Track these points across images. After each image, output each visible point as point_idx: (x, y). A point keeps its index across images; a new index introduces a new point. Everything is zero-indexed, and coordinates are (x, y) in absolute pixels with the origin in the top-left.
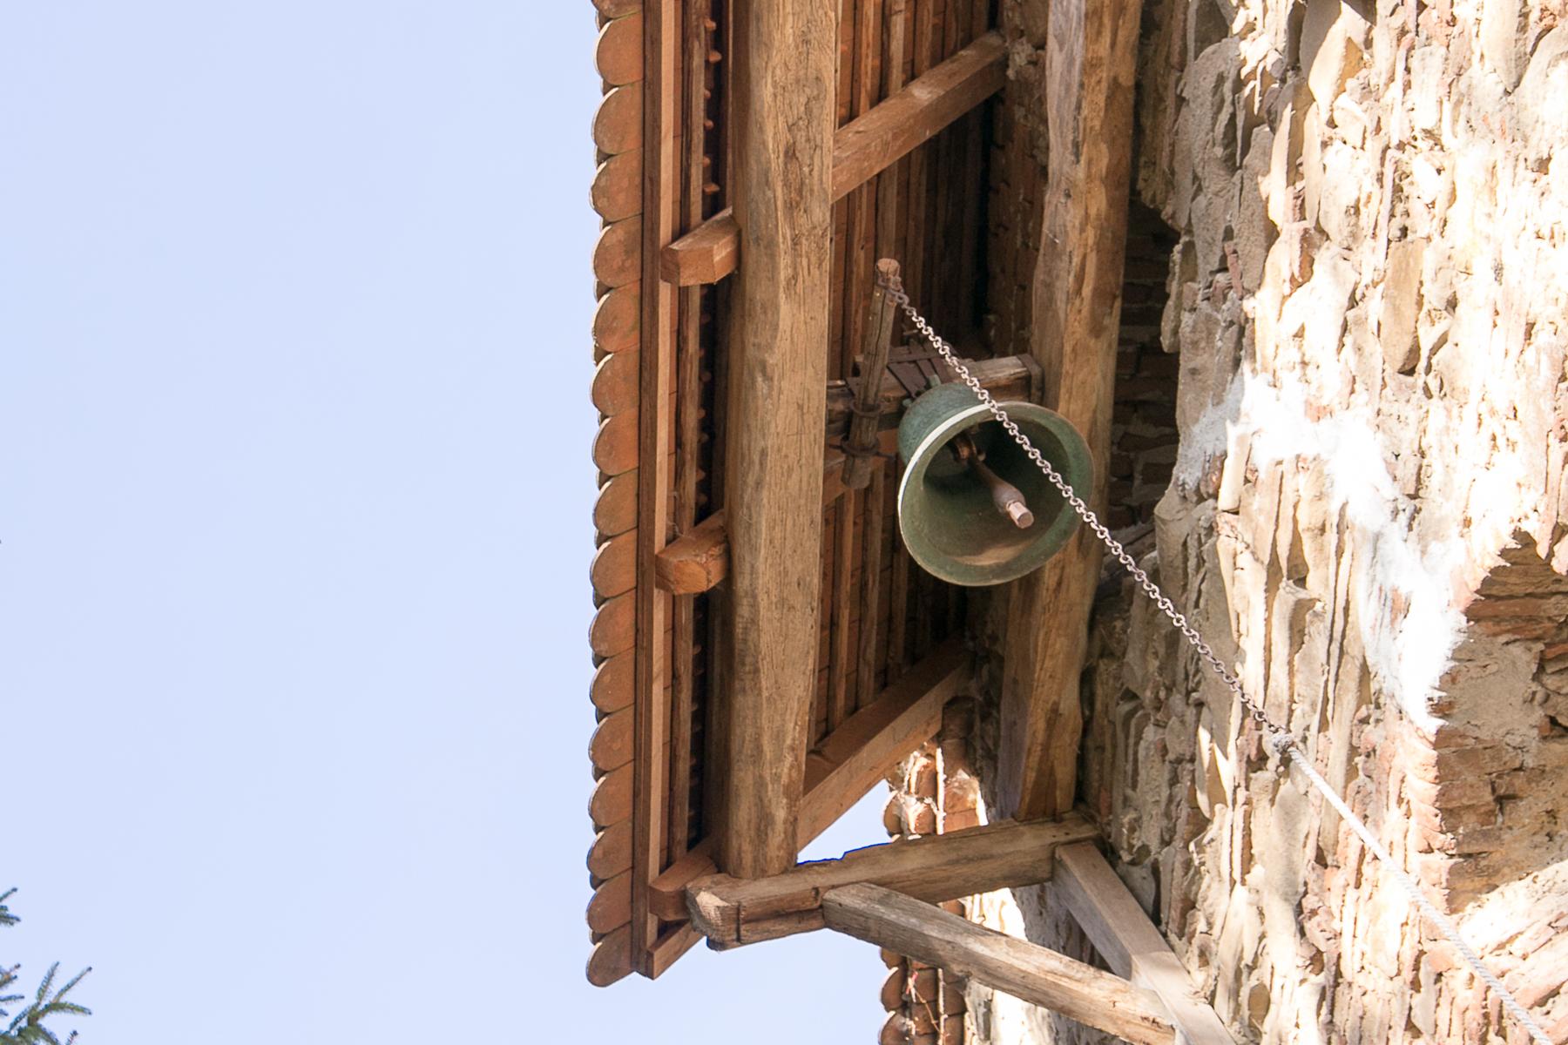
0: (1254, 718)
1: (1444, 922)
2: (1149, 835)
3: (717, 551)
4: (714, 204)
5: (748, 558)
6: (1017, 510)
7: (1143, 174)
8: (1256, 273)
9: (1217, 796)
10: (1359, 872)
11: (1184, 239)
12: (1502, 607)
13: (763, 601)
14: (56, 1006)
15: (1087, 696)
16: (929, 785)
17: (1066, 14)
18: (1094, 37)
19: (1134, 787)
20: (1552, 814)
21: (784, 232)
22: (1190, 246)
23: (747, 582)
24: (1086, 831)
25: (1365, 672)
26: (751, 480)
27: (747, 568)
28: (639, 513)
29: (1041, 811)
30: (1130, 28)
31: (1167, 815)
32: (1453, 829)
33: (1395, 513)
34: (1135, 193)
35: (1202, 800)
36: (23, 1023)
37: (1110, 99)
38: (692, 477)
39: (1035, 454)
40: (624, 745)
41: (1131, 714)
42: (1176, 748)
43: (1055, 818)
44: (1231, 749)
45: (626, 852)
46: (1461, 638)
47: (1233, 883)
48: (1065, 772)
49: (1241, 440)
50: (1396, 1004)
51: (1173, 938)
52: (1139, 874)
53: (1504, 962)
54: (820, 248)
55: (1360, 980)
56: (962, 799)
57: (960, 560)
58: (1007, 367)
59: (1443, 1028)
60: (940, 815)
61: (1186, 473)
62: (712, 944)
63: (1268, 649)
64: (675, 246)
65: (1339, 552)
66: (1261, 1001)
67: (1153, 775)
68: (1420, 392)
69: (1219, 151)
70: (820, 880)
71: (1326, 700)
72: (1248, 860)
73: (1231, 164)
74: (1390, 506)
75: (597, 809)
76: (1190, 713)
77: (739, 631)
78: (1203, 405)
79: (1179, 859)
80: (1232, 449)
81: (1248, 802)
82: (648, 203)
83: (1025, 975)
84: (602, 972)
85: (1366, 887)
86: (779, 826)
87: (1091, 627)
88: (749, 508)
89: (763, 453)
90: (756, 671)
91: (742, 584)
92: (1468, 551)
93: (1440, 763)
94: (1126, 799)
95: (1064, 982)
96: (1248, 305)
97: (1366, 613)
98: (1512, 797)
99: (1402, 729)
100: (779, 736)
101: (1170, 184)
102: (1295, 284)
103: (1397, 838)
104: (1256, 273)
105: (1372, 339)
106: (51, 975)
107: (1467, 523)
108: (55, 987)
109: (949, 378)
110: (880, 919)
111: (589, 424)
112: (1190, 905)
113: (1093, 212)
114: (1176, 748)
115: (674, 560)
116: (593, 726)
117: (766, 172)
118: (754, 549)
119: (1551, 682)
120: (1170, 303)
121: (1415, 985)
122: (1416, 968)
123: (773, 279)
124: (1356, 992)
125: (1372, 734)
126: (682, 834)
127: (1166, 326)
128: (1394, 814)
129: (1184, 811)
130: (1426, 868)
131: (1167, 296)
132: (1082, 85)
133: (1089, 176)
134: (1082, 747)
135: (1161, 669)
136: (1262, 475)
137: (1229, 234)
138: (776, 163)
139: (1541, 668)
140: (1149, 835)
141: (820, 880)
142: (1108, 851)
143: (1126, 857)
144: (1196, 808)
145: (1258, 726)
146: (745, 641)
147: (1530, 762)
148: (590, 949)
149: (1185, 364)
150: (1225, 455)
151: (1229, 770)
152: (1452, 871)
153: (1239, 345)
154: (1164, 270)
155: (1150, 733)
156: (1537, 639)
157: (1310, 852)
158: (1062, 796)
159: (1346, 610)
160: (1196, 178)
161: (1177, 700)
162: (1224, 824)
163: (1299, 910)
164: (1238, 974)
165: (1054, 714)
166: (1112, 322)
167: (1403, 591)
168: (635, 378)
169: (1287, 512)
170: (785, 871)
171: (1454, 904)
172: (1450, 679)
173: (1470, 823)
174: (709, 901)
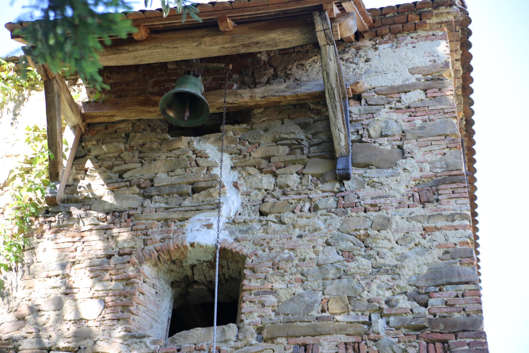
5: (146, 47)
18: (291, 96)
23: (139, 48)
26: (168, 45)
27: (143, 48)
28: (151, 18)
37: (277, 102)
43: (83, 121)
48: (97, 120)
77: (126, 47)
82: (237, 10)
84: (10, 26)
88: (160, 46)
89: (177, 48)
90: (115, 54)
91: (139, 47)
117: (251, 38)
118: (149, 49)
132: (280, 96)
138: (256, 39)
146: (122, 50)
158: (89, 121)
159: (198, 210)
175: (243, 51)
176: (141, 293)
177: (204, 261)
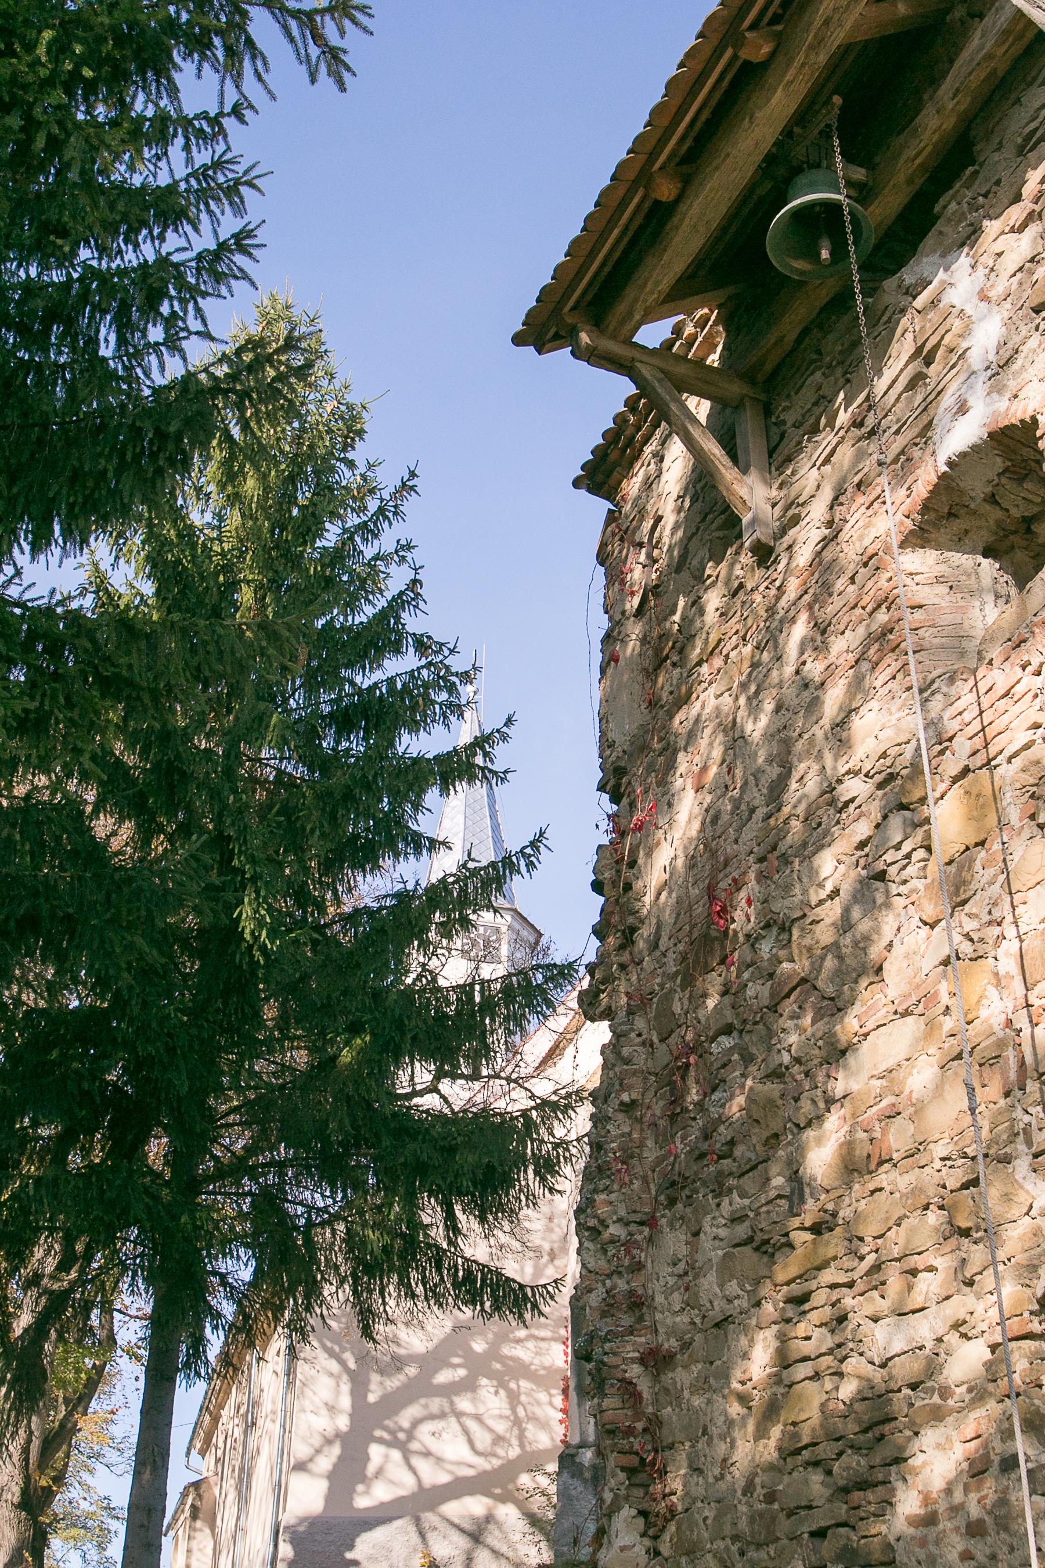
0: (870, 404)
1: (895, 549)
2: (790, 418)
3: (679, 185)
4: (775, 20)
6: (825, 254)
7: (978, 121)
8: (998, 211)
9: (831, 424)
10: (872, 504)
11: (976, 167)
12: (1006, 440)
13: (687, 221)
14: (250, 184)
15: (799, 340)
16: (702, 323)
17: (995, 23)
18: (998, 44)
19: (796, 393)
20: (966, 532)
21: (801, 58)
22: (977, 172)
24: (763, 397)
25: (929, 425)
26: (714, 164)
29: (749, 377)
30: (1018, 49)
31: (803, 416)
32: (923, 515)
33: (988, 368)
34: (968, 128)
35: (823, 421)
36: (231, 183)
38: (689, 143)
39: (851, 239)
40: (586, 248)
41: (815, 361)
42: (825, 391)
43: (753, 382)
44: (850, 410)
45: (559, 296)
46: (980, 442)
47: (814, 465)
48: (769, 367)
49: (943, 282)
50: (852, 566)
51: (773, 469)
52: (774, 430)
53: (908, 581)
54: (812, 75)
55: (844, 545)
56: (714, 338)
57: (788, 260)
58: (859, 174)
59: (866, 589)
60: (700, 339)
61: (908, 275)
62: (572, 353)
63: (894, 382)
64: (747, 34)
65: (953, 367)
66: (796, 520)
67: (807, 395)
68: (1033, 325)
69: (1019, 140)
70: (637, 355)
71: (905, 423)
72: (827, 461)
73: (1021, 151)
74: (987, 364)
75: (559, 270)
76: (842, 381)
77: (668, 227)
78: (935, 251)
79: (797, 438)
80: (935, 282)
81: (843, 438)
83: (702, 449)
84: (519, 340)
85: (870, 512)
86: (634, 322)
87: (822, 310)
89: (728, 155)
91: (682, 208)
92: (1008, 409)
93: (936, 486)
94: (789, 396)
95: (717, 462)
96: (986, 223)
97: (948, 400)
98: (956, 516)
99: (930, 461)
100: (657, 283)
101: (988, 135)
102: (1012, 230)
103: (898, 502)
104: (998, 211)
105: (1029, 285)
106: (253, 166)
107: (1016, 396)
108: (253, 174)
109: (831, 167)
110: (654, 388)
111: (657, 95)
112: (789, 460)
113: (944, 127)
114: (825, 391)
115: (658, 180)
116: (578, 232)
118: (697, 196)
119: (1004, 480)
120: (951, 192)
121: (866, 565)
122: (871, 558)
123: (783, 75)
124: (838, 548)
125: (916, 453)
126: (589, 297)
127: (942, 202)
128: (903, 492)
129: (812, 420)
130: (902, 523)
131: (951, 188)
133: (953, 109)
134: (783, 360)
135: (840, 352)
136: (941, 305)
137: (998, 183)
138: (818, 22)
139: (1003, 473)
140: (790, 418)
141: (637, 355)
142: (767, 411)
143: (774, 420)
144: (818, 422)
145: (869, 411)
147: (972, 506)
148: (520, 327)
149: (939, 225)
150: (930, 283)
151: (843, 418)
152: (911, 531)
153: (969, 237)
154: (957, 176)
155: (818, 376)
156: (1010, 460)
157: (856, 479)
158: (760, 377)
159: (939, 393)
160: (1000, 143)
161: (839, 371)
162: (827, 439)
163: (836, 498)
164: (792, 503)
165: (781, 339)
166: (919, 182)
167: (969, 404)
168: (690, 84)
169: (941, 331)
170: (624, 342)
171: (902, 545)
172: (963, 455)
173: (933, 516)
174: (584, 338)
175: (822, 58)
176: (913, 608)
177: (999, 475)
